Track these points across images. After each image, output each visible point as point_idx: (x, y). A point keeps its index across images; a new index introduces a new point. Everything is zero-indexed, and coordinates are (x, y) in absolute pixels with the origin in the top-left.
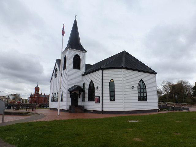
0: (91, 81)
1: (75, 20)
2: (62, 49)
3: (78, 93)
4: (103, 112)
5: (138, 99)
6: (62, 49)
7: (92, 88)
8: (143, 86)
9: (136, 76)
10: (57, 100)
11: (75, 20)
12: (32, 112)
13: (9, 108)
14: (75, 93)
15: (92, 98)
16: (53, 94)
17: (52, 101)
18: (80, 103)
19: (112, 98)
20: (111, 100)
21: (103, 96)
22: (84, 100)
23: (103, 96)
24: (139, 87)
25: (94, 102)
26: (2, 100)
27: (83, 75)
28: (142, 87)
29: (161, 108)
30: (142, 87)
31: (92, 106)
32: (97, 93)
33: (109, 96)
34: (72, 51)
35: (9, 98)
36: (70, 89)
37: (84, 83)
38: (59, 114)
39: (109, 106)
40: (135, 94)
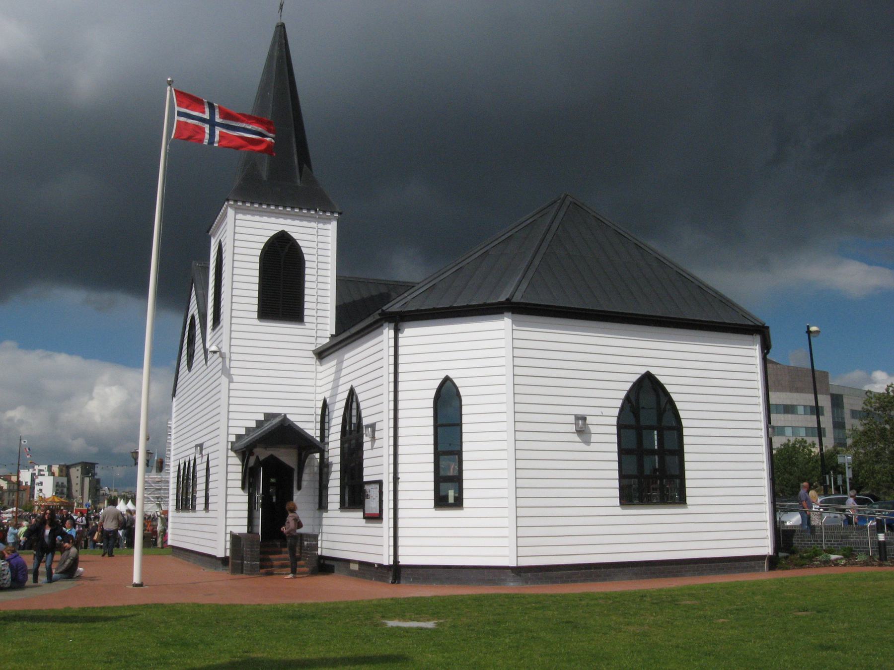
2: (659, 375)
3: (287, 457)
5: (617, 493)
6: (659, 375)
10: (194, 508)
16: (182, 467)
20: (441, 502)
22: (322, 505)
24: (632, 421)
27: (322, 354)
33: (431, 477)
35: (37, 488)
36: (239, 437)
37: (352, 393)
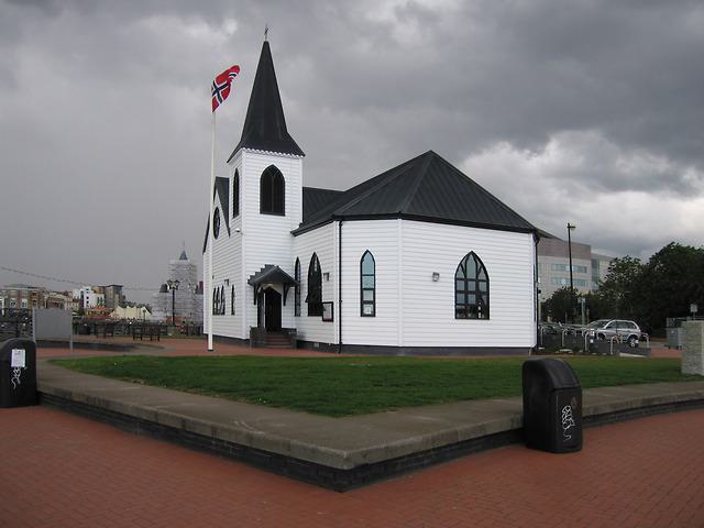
0: (314, 255)
1: (266, 45)
3: (280, 290)
4: (341, 347)
7: (316, 277)
8: (478, 273)
9: (448, 243)
11: (266, 45)
12: (149, 343)
13: (88, 332)
14: (270, 292)
15: (316, 308)
17: (332, 303)
18: (288, 320)
19: (368, 306)
21: (340, 301)
22: (297, 314)
23: (340, 301)
24: (461, 275)
25: (320, 318)
26: (62, 306)
27: (295, 234)
28: (471, 273)
29: (546, 340)
30: (471, 273)
31: (314, 330)
32: (328, 293)
34: (256, 156)
38: (210, 347)
39: (357, 331)
40: (445, 296)
